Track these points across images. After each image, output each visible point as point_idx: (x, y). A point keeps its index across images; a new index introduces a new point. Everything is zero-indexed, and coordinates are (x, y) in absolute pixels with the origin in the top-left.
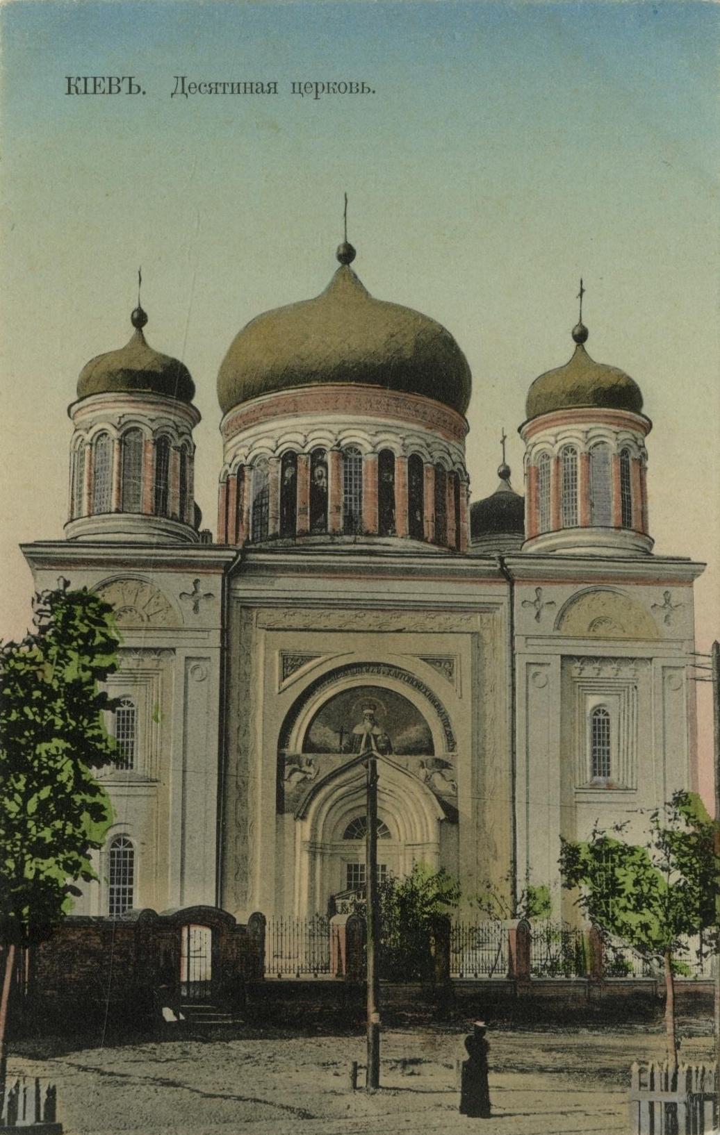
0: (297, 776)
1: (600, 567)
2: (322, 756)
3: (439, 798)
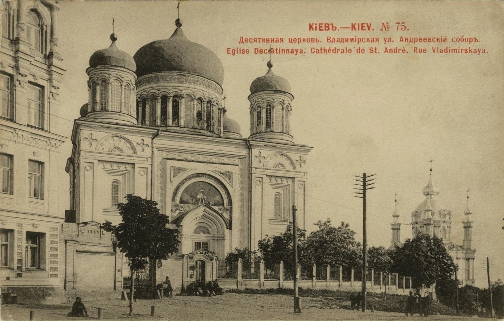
1: (261, 144)
2: (187, 205)
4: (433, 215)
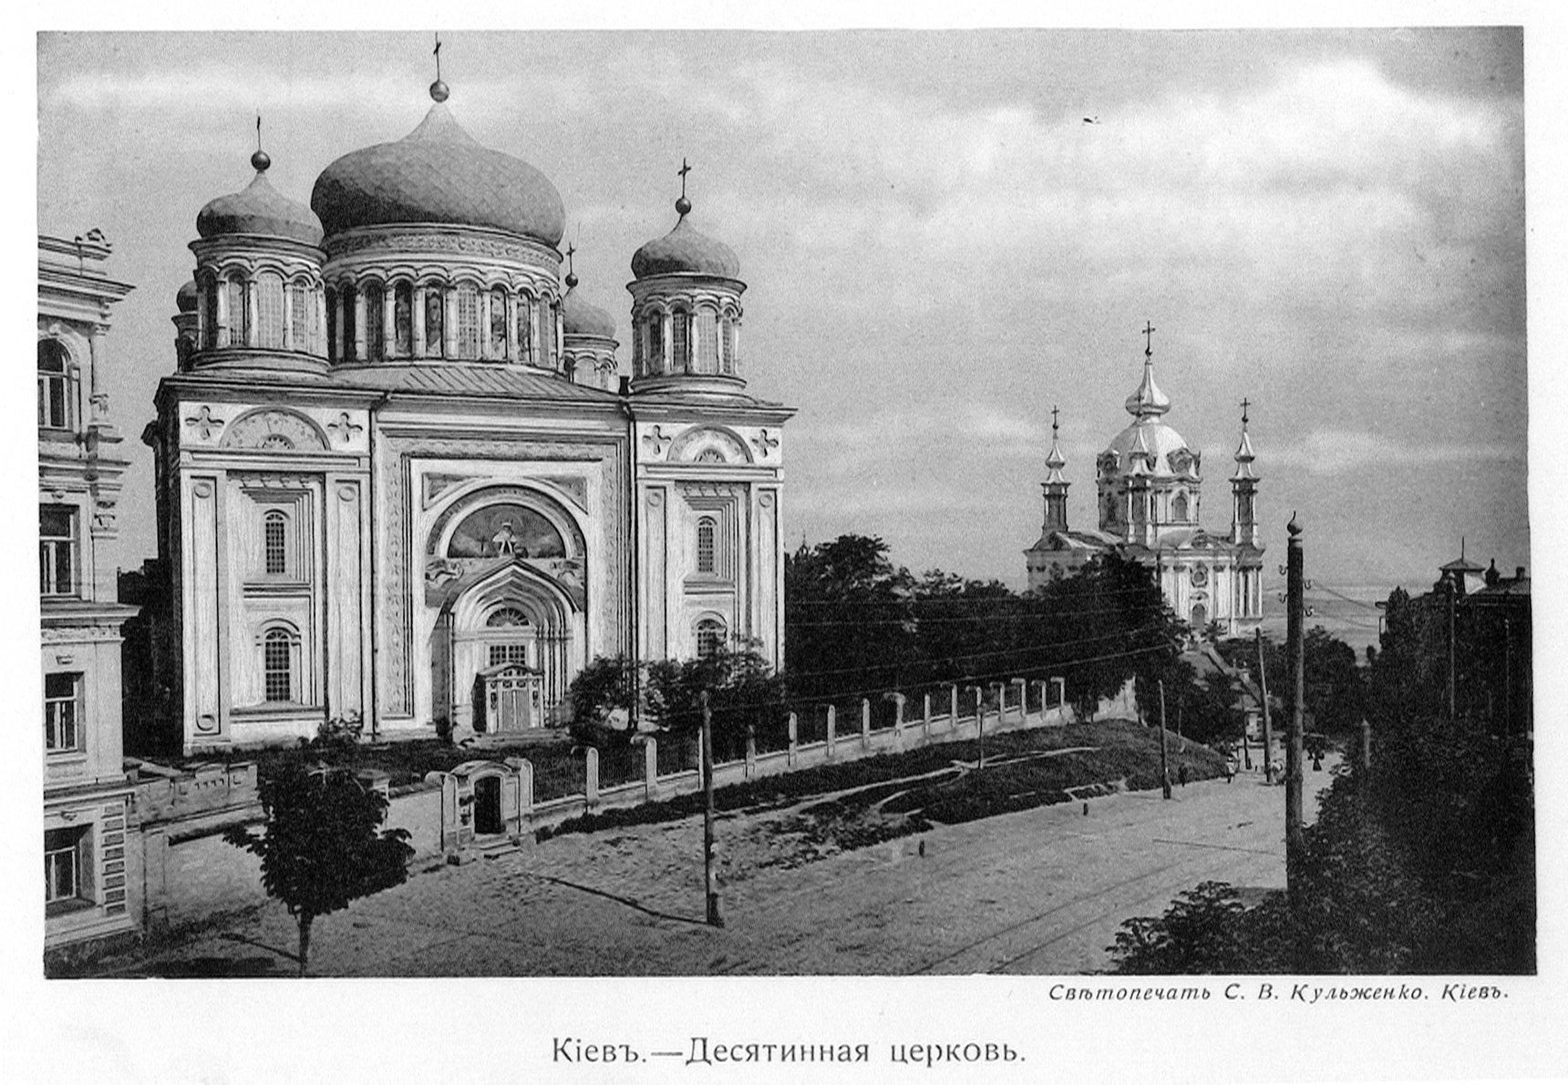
0: (443, 578)
2: (467, 561)
3: (469, 477)
4: (1151, 464)
